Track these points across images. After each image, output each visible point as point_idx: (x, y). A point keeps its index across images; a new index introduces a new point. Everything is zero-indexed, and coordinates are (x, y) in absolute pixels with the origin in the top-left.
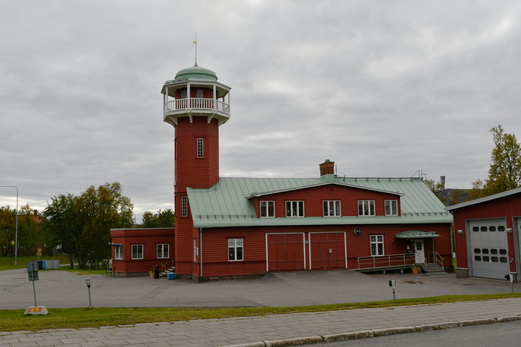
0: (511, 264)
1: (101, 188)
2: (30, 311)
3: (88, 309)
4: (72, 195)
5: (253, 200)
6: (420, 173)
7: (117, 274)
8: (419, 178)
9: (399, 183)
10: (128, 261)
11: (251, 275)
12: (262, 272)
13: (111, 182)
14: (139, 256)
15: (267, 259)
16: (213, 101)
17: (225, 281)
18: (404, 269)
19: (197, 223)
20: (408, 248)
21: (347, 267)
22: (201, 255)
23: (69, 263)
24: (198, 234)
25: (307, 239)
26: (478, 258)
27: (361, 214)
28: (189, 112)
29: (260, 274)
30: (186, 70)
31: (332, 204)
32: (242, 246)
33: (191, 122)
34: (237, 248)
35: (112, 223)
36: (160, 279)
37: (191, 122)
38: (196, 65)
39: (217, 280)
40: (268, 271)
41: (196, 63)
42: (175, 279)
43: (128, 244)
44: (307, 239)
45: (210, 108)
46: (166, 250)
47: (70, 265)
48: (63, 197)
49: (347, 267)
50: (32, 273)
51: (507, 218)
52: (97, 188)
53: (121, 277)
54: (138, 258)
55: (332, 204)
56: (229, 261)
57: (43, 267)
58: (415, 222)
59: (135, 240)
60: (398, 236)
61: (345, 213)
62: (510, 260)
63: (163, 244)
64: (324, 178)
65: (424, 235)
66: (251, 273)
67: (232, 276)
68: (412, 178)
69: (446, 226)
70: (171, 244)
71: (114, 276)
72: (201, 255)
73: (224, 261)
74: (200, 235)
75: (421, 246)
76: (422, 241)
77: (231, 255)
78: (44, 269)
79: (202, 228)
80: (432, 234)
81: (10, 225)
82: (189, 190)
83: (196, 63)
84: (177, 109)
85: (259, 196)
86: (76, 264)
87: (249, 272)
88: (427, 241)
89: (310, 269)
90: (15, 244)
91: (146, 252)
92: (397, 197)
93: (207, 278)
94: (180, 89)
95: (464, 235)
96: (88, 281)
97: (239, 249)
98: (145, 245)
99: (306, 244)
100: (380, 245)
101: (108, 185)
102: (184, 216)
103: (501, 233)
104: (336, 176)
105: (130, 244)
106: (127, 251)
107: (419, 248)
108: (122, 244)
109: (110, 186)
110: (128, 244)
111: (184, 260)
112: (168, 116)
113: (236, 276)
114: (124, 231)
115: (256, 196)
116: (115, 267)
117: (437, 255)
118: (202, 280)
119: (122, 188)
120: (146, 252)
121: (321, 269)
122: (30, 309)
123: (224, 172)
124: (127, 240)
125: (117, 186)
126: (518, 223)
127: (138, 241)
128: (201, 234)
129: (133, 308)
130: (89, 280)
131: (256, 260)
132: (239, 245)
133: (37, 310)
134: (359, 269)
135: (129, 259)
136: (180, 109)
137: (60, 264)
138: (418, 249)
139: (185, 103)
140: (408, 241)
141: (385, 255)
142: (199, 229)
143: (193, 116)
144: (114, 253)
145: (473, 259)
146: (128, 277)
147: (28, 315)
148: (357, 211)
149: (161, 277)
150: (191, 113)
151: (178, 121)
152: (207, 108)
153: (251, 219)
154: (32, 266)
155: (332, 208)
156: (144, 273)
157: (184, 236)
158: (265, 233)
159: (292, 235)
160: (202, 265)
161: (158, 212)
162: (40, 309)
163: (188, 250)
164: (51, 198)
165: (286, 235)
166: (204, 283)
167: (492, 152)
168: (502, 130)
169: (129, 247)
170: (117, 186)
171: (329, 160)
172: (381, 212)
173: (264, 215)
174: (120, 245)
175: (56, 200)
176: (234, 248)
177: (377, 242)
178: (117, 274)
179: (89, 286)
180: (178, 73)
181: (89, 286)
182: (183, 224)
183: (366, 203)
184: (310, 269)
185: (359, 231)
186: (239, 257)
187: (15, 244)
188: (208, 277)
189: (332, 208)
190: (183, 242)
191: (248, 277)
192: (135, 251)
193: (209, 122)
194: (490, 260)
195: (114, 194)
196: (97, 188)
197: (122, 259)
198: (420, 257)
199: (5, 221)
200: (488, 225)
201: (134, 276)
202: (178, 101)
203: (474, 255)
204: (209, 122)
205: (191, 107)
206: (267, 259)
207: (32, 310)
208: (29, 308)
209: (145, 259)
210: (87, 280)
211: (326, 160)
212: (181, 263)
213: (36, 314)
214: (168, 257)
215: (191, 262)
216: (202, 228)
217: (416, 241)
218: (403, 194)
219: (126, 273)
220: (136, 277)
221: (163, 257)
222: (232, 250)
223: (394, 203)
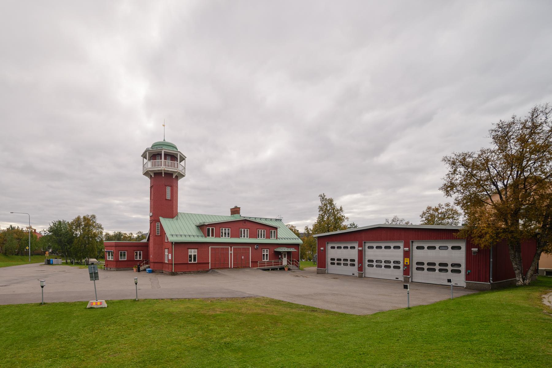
0: (359, 267)
1: (84, 217)
2: (92, 305)
3: (135, 300)
4: (65, 221)
5: (201, 227)
6: (280, 217)
7: (109, 269)
8: (279, 219)
9: (271, 221)
10: (117, 261)
13: (90, 214)
15: (210, 262)
16: (178, 163)
17: (187, 274)
18: (271, 269)
19: (171, 239)
20: (280, 256)
21: (250, 267)
22: (173, 259)
23: (64, 260)
24: (171, 246)
25: (231, 251)
26: (354, 260)
27: (259, 237)
30: (158, 142)
31: (244, 231)
32: (196, 254)
33: (163, 176)
34: (194, 255)
36: (141, 272)
37: (163, 176)
38: (164, 140)
39: (182, 274)
41: (164, 139)
44: (231, 251)
46: (140, 255)
47: (65, 261)
48: (60, 222)
49: (250, 267)
50: (94, 274)
51: (359, 242)
52: (82, 217)
53: (112, 271)
54: (123, 259)
55: (244, 231)
56: (189, 262)
57: (51, 263)
58: (284, 243)
60: (276, 250)
61: (251, 236)
62: (359, 265)
63: (139, 251)
64: (233, 216)
65: (289, 250)
68: (276, 219)
69: (296, 245)
72: (173, 259)
73: (186, 262)
75: (285, 256)
76: (286, 253)
77: (190, 259)
78: (51, 264)
79: (174, 242)
80: (293, 249)
81: (20, 237)
82: (161, 219)
83: (164, 139)
84: (152, 167)
85: (207, 224)
86: (69, 261)
88: (289, 253)
90: (29, 249)
92: (276, 228)
94: (155, 154)
95: (325, 251)
96: (136, 280)
100: (267, 255)
101: (88, 216)
103: (353, 250)
104: (240, 215)
107: (285, 257)
108: (113, 251)
109: (90, 217)
112: (149, 171)
115: (205, 224)
116: (107, 265)
117: (295, 260)
118: (173, 274)
119: (96, 218)
121: (238, 268)
122: (92, 303)
123: (179, 210)
125: (94, 217)
126: (413, 245)
128: (173, 246)
129: (169, 299)
130: (137, 279)
131: (204, 262)
132: (195, 253)
133: (99, 304)
134: (259, 268)
135: (118, 260)
136: (155, 167)
137: (62, 260)
138: (284, 257)
139: (159, 164)
140: (279, 253)
141: (269, 260)
142: (172, 243)
144: (107, 256)
145: (329, 264)
147: (91, 308)
148: (256, 236)
149: (141, 271)
150: (164, 170)
151: (154, 175)
152: (174, 168)
153: (201, 238)
154: (93, 268)
155: (244, 233)
158: (209, 247)
159: (223, 248)
162: (101, 303)
164: (52, 222)
168: (324, 196)
170: (94, 217)
171: (237, 206)
172: (268, 237)
173: (209, 235)
174: (111, 252)
175: (55, 223)
176: (191, 255)
177: (265, 253)
178: (109, 269)
179: (136, 284)
180: (154, 144)
181: (136, 284)
183: (262, 231)
185: (258, 247)
186: (195, 260)
187: (29, 249)
189: (244, 233)
192: (121, 255)
193: (174, 177)
194: (342, 265)
195: (92, 221)
196: (82, 217)
198: (285, 261)
199: (16, 235)
200: (342, 246)
202: (154, 162)
203: (367, 263)
204: (174, 177)
206: (210, 262)
207: (94, 304)
208: (91, 302)
210: (135, 279)
213: (97, 307)
214: (142, 259)
215: (163, 263)
216: (174, 242)
217: (284, 253)
218: (280, 227)
221: (138, 259)
222: (190, 256)
223: (274, 232)
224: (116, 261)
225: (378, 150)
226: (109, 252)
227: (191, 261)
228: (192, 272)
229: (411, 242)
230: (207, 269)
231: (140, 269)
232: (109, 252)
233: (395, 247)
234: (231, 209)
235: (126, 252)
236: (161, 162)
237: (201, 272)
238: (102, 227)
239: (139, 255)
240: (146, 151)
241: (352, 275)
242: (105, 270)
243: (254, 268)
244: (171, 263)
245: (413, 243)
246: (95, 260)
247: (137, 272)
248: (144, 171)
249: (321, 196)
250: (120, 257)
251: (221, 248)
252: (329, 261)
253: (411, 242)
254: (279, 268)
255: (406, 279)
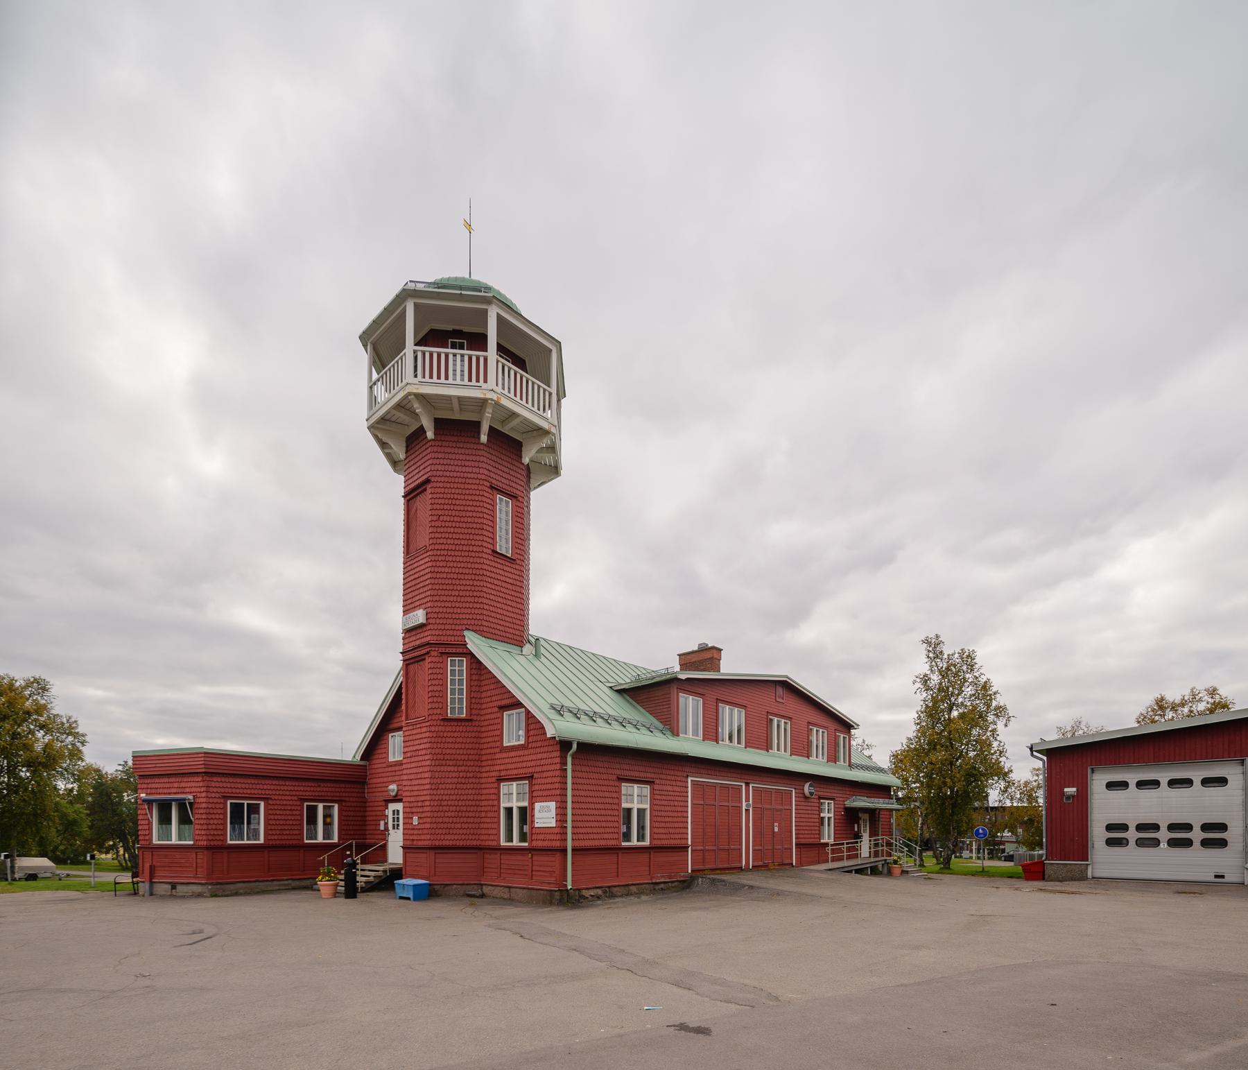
11: (665, 883)
12: (682, 874)
14: (251, 835)
15: (690, 843)
16: (486, 359)
22: (569, 824)
24: (558, 760)
26: (1110, 842)
28: (495, 397)
29: (679, 879)
32: (647, 806)
35: (39, 766)
39: (598, 898)
40: (692, 871)
42: (425, 899)
43: (217, 795)
45: (478, 380)
49: (794, 864)
54: (248, 839)
59: (239, 786)
60: (848, 803)
66: (662, 877)
67: (628, 885)
70: (344, 804)
71: (151, 894)
72: (569, 824)
74: (565, 764)
79: (579, 744)
87: (659, 875)
89: (751, 867)
91: (274, 822)
93: (577, 892)
95: (1083, 799)
97: (641, 812)
98: (270, 802)
99: (746, 810)
100: (829, 818)
102: (457, 716)
105: (224, 797)
106: (213, 816)
108: (191, 797)
110: (217, 795)
111: (454, 843)
112: (417, 395)
113: (637, 886)
114: (203, 755)
120: (274, 822)
124: (213, 784)
126: (1094, 778)
127: (249, 791)
135: (220, 843)
143: (435, 419)
144: (150, 824)
146: (216, 896)
156: (267, 883)
157: (454, 775)
158: (688, 776)
160: (573, 855)
161: (120, 765)
163: (467, 814)
165: (719, 785)
166: (575, 908)
167: (914, 682)
169: (218, 806)
182: (450, 740)
184: (751, 867)
188: (579, 890)
190: (449, 792)
191: (657, 887)
197: (192, 843)
201: (236, 894)
205: (416, 376)
209: (271, 842)
211: (700, 645)
212: (504, 852)
216: (579, 744)
219: (212, 884)
220: (241, 894)
221: (320, 839)
222: (509, 811)
224: (207, 848)
225: (797, 613)
226: (165, 808)
227: (627, 836)
228: (634, 889)
229: (1089, 771)
230: (682, 876)
231: (358, 879)
232: (165, 808)
233: (1141, 784)
234: (679, 655)
235: (262, 804)
236: (482, 360)
237: (662, 886)
238: (80, 730)
239: (325, 823)
240: (405, 295)
241: (1213, 879)
242: (135, 893)
243: (812, 867)
244: (557, 844)
245: (1094, 775)
246: (44, 862)
247: (342, 900)
248: (375, 409)
249: (927, 641)
250: (233, 829)
251: (723, 786)
252: (1098, 834)
253: (1089, 771)
254: (871, 867)
255: (648, 891)
